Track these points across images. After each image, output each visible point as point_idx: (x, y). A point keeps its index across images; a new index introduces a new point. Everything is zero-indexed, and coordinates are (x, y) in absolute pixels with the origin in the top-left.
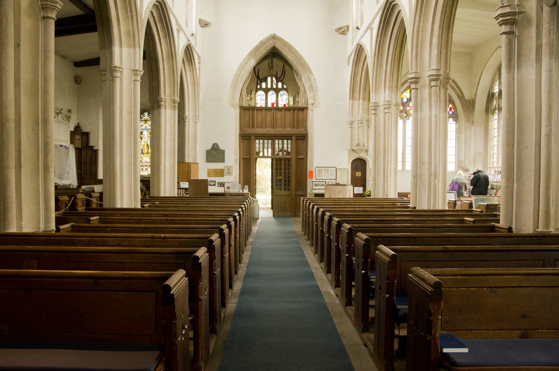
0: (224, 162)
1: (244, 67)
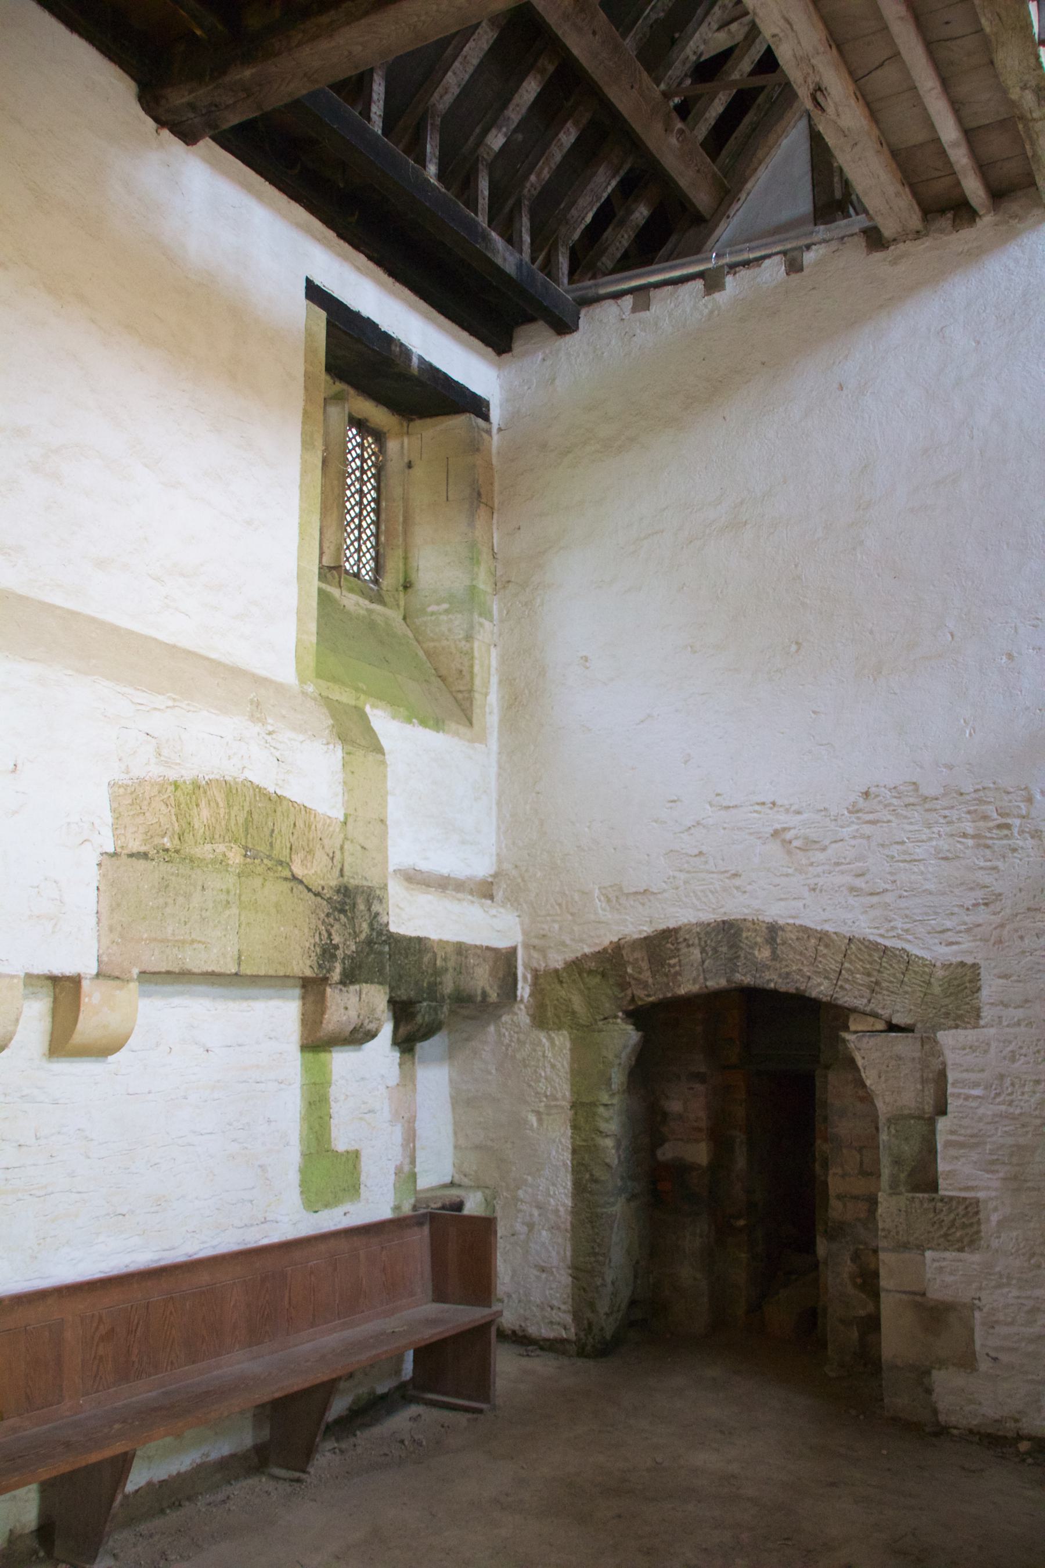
0: (357, 1154)
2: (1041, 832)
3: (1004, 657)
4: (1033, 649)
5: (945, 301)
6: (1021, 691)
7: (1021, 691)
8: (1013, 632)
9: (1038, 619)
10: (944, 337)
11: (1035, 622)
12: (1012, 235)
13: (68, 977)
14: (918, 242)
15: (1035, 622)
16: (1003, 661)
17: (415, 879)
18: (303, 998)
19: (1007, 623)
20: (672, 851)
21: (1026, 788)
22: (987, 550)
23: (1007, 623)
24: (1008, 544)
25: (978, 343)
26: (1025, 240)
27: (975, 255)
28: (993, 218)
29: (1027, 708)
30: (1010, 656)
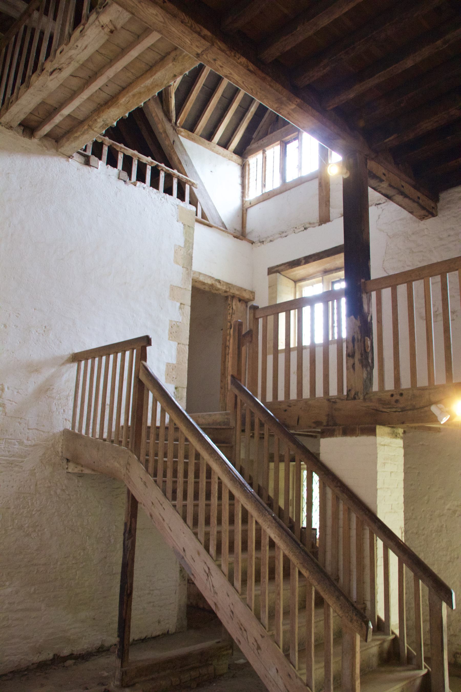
1: (124, 89)
2: (5, 404)
3: (3, 325)
4: (15, 326)
5: (12, 162)
6: (7, 342)
7: (7, 342)
8: (8, 316)
9: (19, 314)
10: (8, 177)
11: (18, 315)
12: (42, 153)
13: (40, 103)
14: (7, 130)
15: (18, 315)
16: (2, 327)
17: (264, 186)
18: (219, 218)
19: (7, 311)
20: (377, 221)
21: (2, 384)
22: (5, 277)
23: (7, 311)
24: (14, 278)
25: (21, 188)
26: (47, 159)
27: (27, 151)
28: (38, 142)
29: (8, 350)
30: (5, 326)
